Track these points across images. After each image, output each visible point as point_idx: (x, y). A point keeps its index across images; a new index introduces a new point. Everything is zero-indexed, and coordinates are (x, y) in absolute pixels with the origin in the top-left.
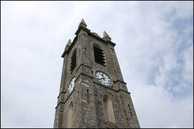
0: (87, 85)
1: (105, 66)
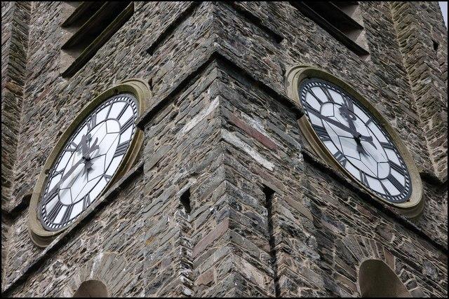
0: (260, 150)
1: (361, 52)
